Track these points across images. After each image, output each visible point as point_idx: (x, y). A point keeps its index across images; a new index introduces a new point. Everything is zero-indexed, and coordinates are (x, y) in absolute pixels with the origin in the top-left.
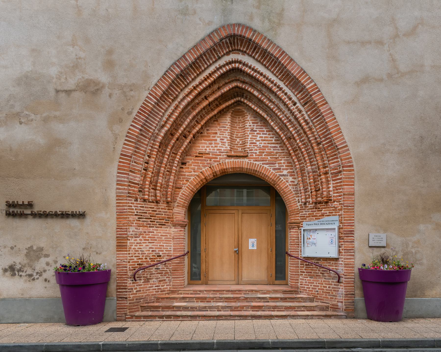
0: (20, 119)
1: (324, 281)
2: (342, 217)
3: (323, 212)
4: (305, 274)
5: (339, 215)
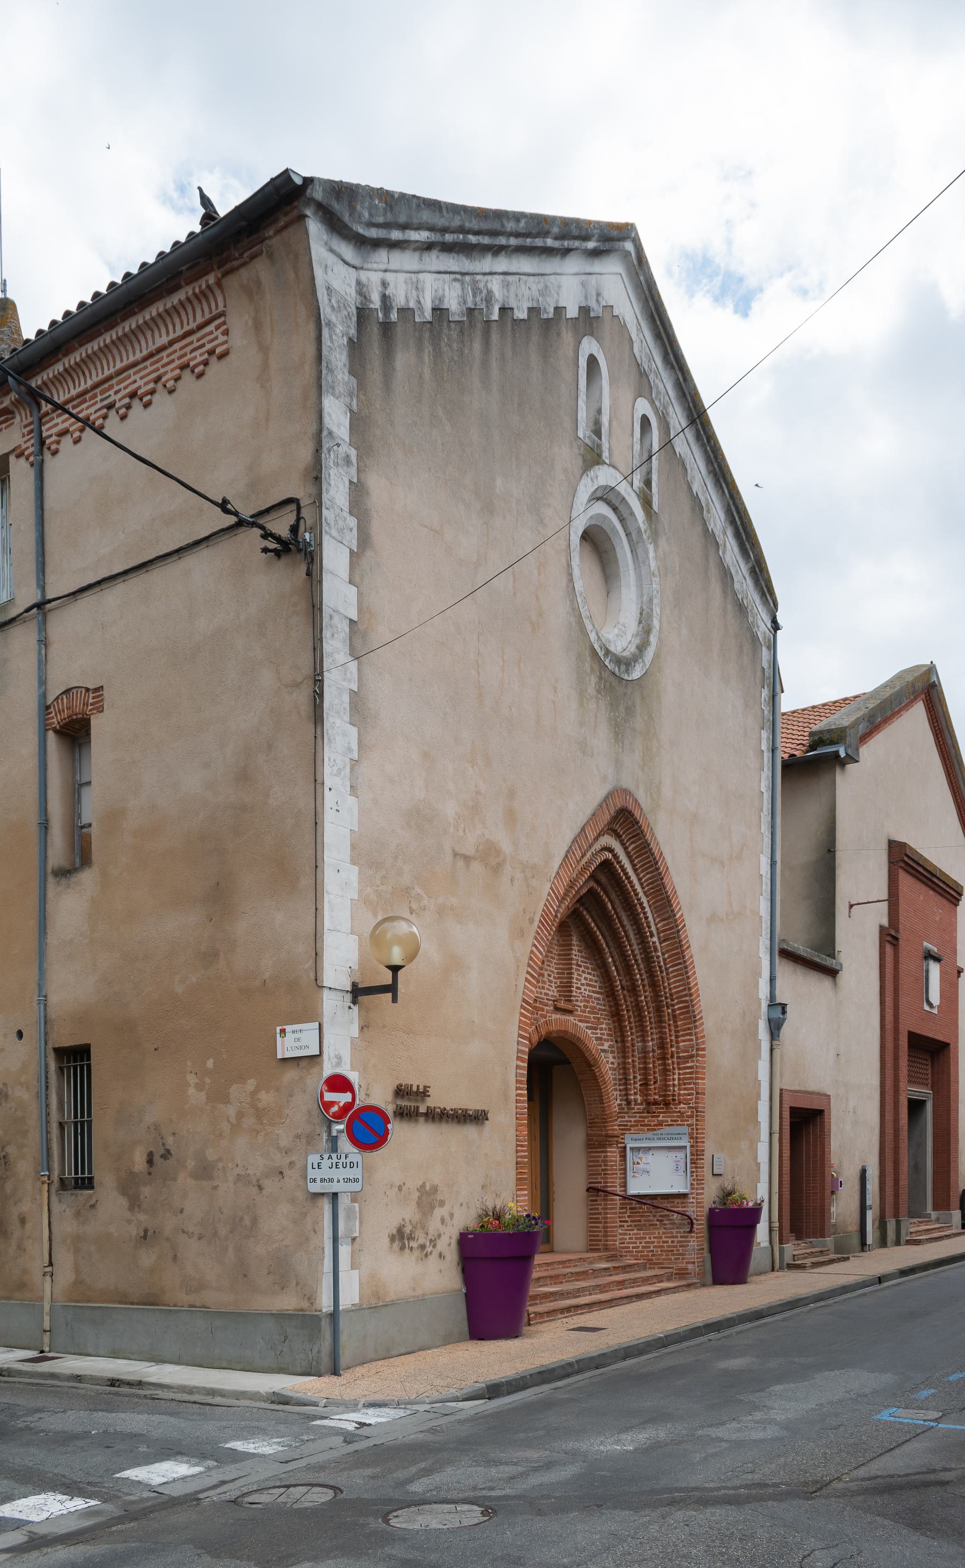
0: (410, 902)
1: (664, 1233)
2: (692, 1129)
3: (660, 1118)
4: (629, 1223)
5: (689, 1125)
